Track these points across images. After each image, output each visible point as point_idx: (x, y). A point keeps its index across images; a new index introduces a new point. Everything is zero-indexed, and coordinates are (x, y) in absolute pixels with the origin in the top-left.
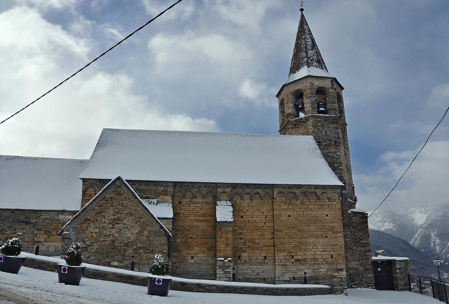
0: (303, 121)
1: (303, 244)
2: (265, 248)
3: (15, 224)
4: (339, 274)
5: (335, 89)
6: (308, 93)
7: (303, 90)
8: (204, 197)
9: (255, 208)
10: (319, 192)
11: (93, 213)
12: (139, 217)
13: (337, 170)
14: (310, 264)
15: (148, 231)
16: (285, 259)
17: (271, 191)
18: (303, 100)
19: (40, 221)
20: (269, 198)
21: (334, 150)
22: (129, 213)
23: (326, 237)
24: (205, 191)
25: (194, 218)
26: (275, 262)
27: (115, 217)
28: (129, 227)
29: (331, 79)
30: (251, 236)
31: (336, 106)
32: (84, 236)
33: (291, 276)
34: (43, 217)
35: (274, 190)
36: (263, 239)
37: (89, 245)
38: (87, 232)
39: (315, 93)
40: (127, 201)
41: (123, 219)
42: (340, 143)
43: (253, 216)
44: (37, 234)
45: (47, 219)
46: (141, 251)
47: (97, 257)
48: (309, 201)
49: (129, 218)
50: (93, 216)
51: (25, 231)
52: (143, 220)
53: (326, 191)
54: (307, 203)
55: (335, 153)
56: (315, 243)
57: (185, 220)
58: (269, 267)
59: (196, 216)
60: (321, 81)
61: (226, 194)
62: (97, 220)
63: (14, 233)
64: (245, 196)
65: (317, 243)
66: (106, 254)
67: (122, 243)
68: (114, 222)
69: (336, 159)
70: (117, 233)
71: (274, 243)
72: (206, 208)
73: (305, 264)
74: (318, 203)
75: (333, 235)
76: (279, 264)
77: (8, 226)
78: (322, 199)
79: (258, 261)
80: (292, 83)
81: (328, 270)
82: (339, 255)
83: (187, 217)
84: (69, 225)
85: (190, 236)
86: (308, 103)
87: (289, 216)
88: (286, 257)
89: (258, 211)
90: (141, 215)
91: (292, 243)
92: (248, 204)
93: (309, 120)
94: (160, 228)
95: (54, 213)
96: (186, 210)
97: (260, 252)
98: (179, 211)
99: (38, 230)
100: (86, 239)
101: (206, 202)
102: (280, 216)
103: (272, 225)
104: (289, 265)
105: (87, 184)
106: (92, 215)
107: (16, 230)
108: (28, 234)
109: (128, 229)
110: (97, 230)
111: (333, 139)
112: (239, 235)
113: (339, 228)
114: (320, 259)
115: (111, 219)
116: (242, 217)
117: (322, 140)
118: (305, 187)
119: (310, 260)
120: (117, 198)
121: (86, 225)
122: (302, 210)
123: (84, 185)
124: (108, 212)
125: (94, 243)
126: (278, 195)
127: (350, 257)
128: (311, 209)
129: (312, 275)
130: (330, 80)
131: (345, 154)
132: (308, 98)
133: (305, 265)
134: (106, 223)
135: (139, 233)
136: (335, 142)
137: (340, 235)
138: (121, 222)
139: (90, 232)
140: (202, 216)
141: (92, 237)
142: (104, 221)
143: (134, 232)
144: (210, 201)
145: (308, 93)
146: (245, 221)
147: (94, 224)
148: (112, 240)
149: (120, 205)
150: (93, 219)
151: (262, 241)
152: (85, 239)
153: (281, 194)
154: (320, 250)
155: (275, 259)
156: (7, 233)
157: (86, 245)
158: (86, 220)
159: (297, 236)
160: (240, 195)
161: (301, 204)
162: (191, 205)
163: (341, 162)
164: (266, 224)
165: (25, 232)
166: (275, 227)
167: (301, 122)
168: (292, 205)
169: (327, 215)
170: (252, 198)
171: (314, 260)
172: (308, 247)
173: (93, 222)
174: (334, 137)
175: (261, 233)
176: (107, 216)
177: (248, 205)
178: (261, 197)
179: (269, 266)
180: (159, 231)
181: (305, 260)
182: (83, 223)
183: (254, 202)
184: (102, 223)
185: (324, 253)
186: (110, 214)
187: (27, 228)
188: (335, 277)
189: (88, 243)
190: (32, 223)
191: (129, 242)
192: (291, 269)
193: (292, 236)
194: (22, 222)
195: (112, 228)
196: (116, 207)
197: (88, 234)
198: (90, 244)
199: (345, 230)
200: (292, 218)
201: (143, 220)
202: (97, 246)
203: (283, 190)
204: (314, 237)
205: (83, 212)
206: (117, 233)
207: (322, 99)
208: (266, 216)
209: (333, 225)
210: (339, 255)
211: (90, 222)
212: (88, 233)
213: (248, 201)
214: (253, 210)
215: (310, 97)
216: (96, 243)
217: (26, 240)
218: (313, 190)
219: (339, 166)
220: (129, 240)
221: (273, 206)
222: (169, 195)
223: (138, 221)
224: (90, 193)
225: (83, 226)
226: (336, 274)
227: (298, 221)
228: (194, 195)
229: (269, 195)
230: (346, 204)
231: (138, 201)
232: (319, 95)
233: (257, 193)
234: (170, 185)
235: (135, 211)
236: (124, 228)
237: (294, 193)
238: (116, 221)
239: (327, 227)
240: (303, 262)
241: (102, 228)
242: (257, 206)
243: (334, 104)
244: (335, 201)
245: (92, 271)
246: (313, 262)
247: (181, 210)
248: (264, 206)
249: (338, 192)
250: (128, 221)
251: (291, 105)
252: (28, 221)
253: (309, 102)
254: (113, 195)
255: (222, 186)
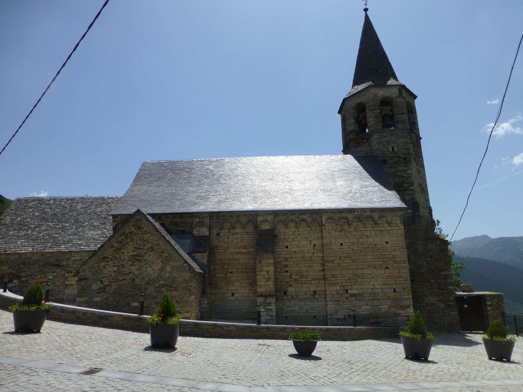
1: (358, 277)
2: (314, 282)
3: (45, 267)
4: (404, 312)
5: (404, 99)
8: (244, 227)
9: (302, 237)
10: (376, 216)
11: (111, 250)
12: (161, 252)
13: (408, 190)
14: (369, 299)
15: (171, 266)
16: (337, 294)
17: (319, 217)
18: (365, 114)
19: (71, 263)
20: (317, 225)
21: (404, 168)
22: (150, 248)
23: (387, 268)
24: (244, 220)
25: (234, 251)
26: (326, 298)
27: (135, 253)
28: (150, 263)
29: (399, 87)
30: (298, 269)
31: (405, 117)
32: (102, 276)
33: (346, 314)
34: (74, 259)
35: (323, 216)
36: (312, 271)
37: (107, 286)
38: (105, 271)
39: (379, 104)
40: (149, 235)
41: (144, 254)
42: (410, 160)
43: (299, 246)
44: (67, 277)
45: (77, 260)
46: (163, 289)
47: (116, 298)
48: (364, 226)
49: (150, 253)
50: (112, 254)
51: (56, 274)
52: (165, 255)
53: (384, 214)
54: (362, 229)
55: (404, 171)
56: (373, 275)
57: (224, 253)
58: (320, 303)
59: (236, 248)
60: (386, 90)
61: (267, 222)
62: (115, 258)
63: (45, 277)
64: (290, 223)
65: (376, 275)
66: (126, 294)
67: (143, 281)
68: (136, 258)
69: (405, 178)
70: (137, 270)
71: (324, 275)
72: (247, 239)
73: (362, 300)
74: (375, 229)
75: (395, 265)
76: (331, 300)
77: (38, 270)
78: (381, 224)
79: (306, 296)
81: (390, 307)
82: (404, 289)
83: (225, 249)
84: (85, 265)
85: (230, 270)
87: (341, 244)
88: (339, 291)
89: (305, 239)
90: (164, 249)
91: (346, 276)
92: (294, 232)
94: (183, 262)
95: (85, 253)
96: (225, 242)
97: (308, 286)
98: (217, 244)
99: (68, 272)
100: (104, 279)
101: (247, 232)
102: (330, 245)
103: (321, 255)
104: (342, 300)
106: (110, 253)
107: (46, 273)
108: (59, 278)
109: (149, 265)
110: (115, 269)
111: (402, 155)
112: (285, 267)
113: (403, 257)
114: (380, 294)
115: (130, 256)
116: (287, 247)
117: (389, 157)
118: (358, 211)
119: (368, 295)
120: (137, 232)
121: (103, 263)
122: (356, 237)
124: (127, 248)
125: (112, 282)
126: (328, 221)
127: (428, 292)
128: (367, 236)
129: (372, 312)
130: (397, 88)
131: (419, 172)
132: (371, 110)
133: (362, 301)
134: (126, 260)
135: (163, 269)
136: (405, 159)
137: (405, 265)
138: (142, 258)
139: (108, 271)
140: (242, 248)
141: (110, 276)
142: (124, 258)
143: (155, 269)
144: (251, 231)
145: (371, 105)
146: (290, 251)
147: (112, 262)
148: (131, 278)
149: (140, 240)
150: (111, 257)
151: (311, 274)
152: (102, 279)
153: (330, 220)
154: (380, 283)
155: (326, 294)
156: (37, 277)
157: (104, 285)
158: (104, 258)
159: (351, 267)
160: (284, 223)
161: (354, 231)
162: (230, 236)
163: (412, 182)
164: (315, 254)
165: (56, 276)
166: (325, 258)
168: (343, 232)
169: (387, 243)
170: (298, 226)
171: (373, 295)
172: (365, 280)
173: (111, 260)
174: (403, 154)
175: (309, 265)
176: (127, 252)
177: (294, 234)
178: (307, 224)
179: (320, 302)
180: (183, 266)
181: (362, 295)
182: (100, 262)
183: (300, 230)
184: (121, 261)
185: (386, 286)
186: (129, 251)
187: (57, 272)
188: (399, 315)
189: (106, 283)
190: (63, 266)
191: (151, 279)
192: (345, 306)
193: (346, 267)
194: (53, 265)
195: (132, 265)
196: (136, 242)
197: (106, 273)
198: (108, 284)
199: (420, 260)
200: (344, 246)
201: (165, 255)
202: (116, 286)
203: (333, 215)
204: (372, 268)
205: (100, 250)
206: (137, 270)
207: (388, 111)
208: (314, 245)
209: (394, 253)
210: (404, 289)
211: (108, 260)
212: (106, 273)
213: (293, 229)
214: (300, 239)
215: (373, 109)
216: (115, 282)
217: (57, 284)
218: (368, 214)
219: (410, 186)
220: (151, 277)
221: (322, 234)
222: (205, 226)
223: (160, 256)
225: (101, 265)
226: (400, 312)
227: (352, 250)
228: (233, 226)
229: (317, 221)
230: (420, 229)
231: (160, 234)
232: (384, 107)
233: (303, 220)
234: (206, 216)
235: (157, 245)
236: (145, 265)
237: (346, 218)
238: (136, 257)
239: (387, 256)
240: (360, 298)
241: (121, 266)
242: (304, 235)
243: (402, 115)
244: (397, 226)
245: (97, 313)
246: (372, 298)
247: (219, 242)
248: (312, 234)
249: (400, 216)
250: (150, 257)
251: (353, 121)
252: (59, 263)
253: (372, 115)
254: (133, 229)
255: (263, 213)
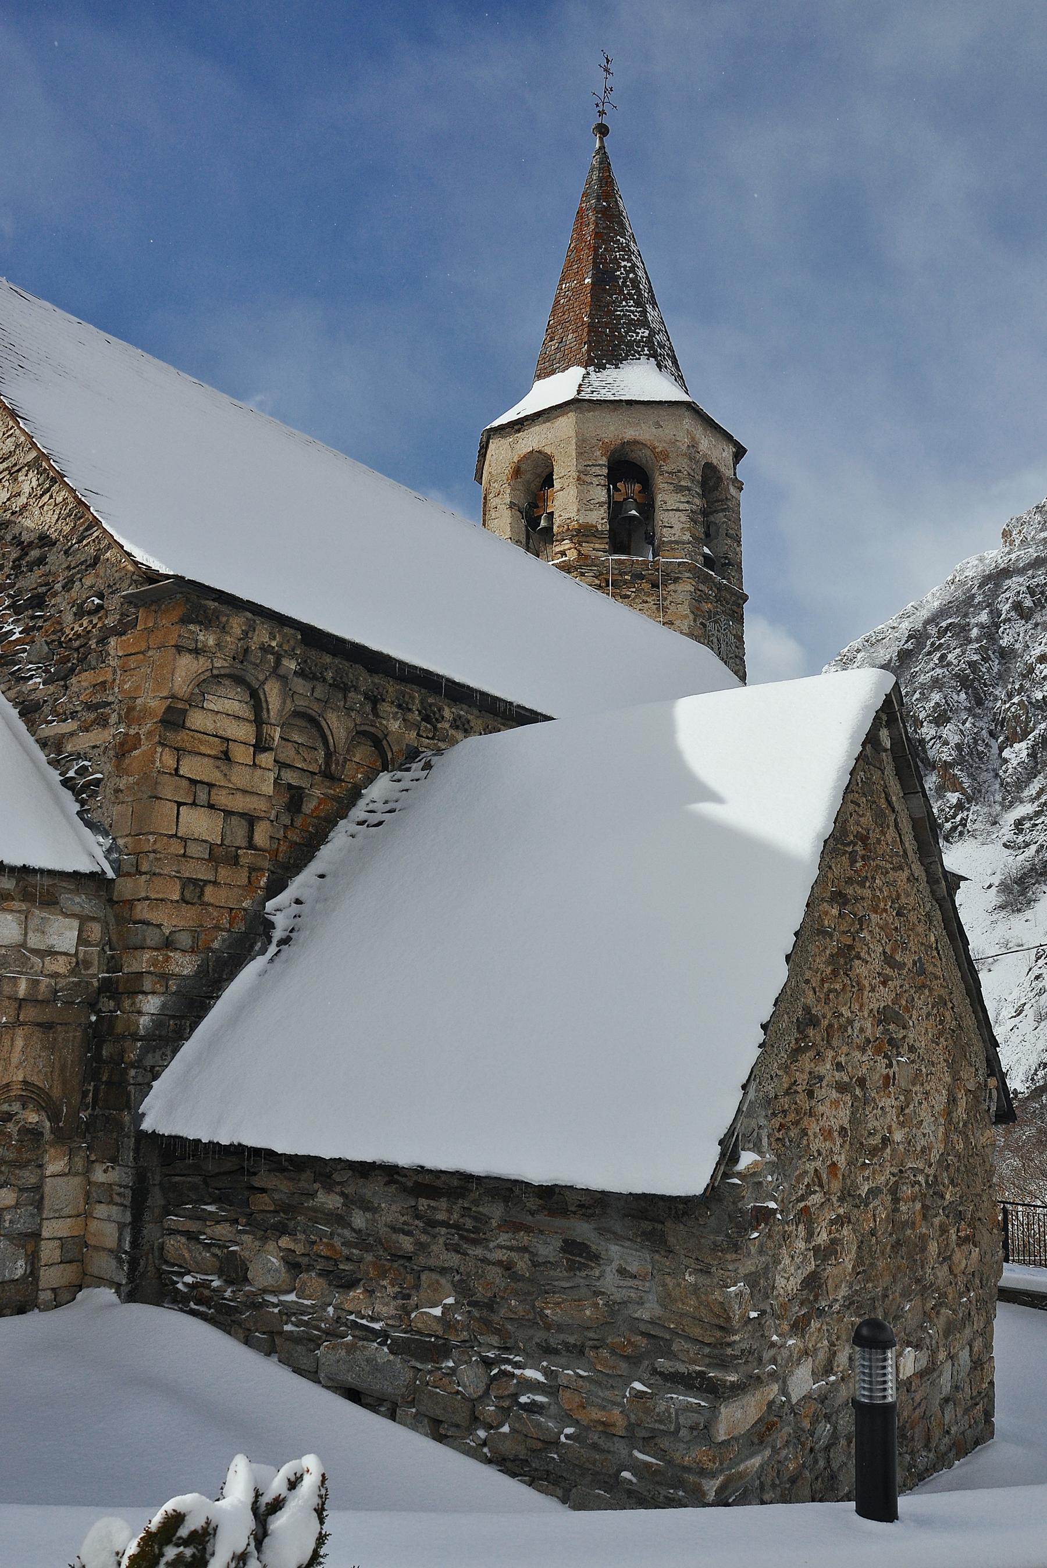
0: (651, 577)
6: (679, 471)
7: (661, 452)
80: (611, 407)
86: (676, 510)
93: (676, 580)
105: (211, 642)
123: (190, 651)
145: (679, 471)
167: (641, 577)
224: (221, 733)
253: (682, 507)
